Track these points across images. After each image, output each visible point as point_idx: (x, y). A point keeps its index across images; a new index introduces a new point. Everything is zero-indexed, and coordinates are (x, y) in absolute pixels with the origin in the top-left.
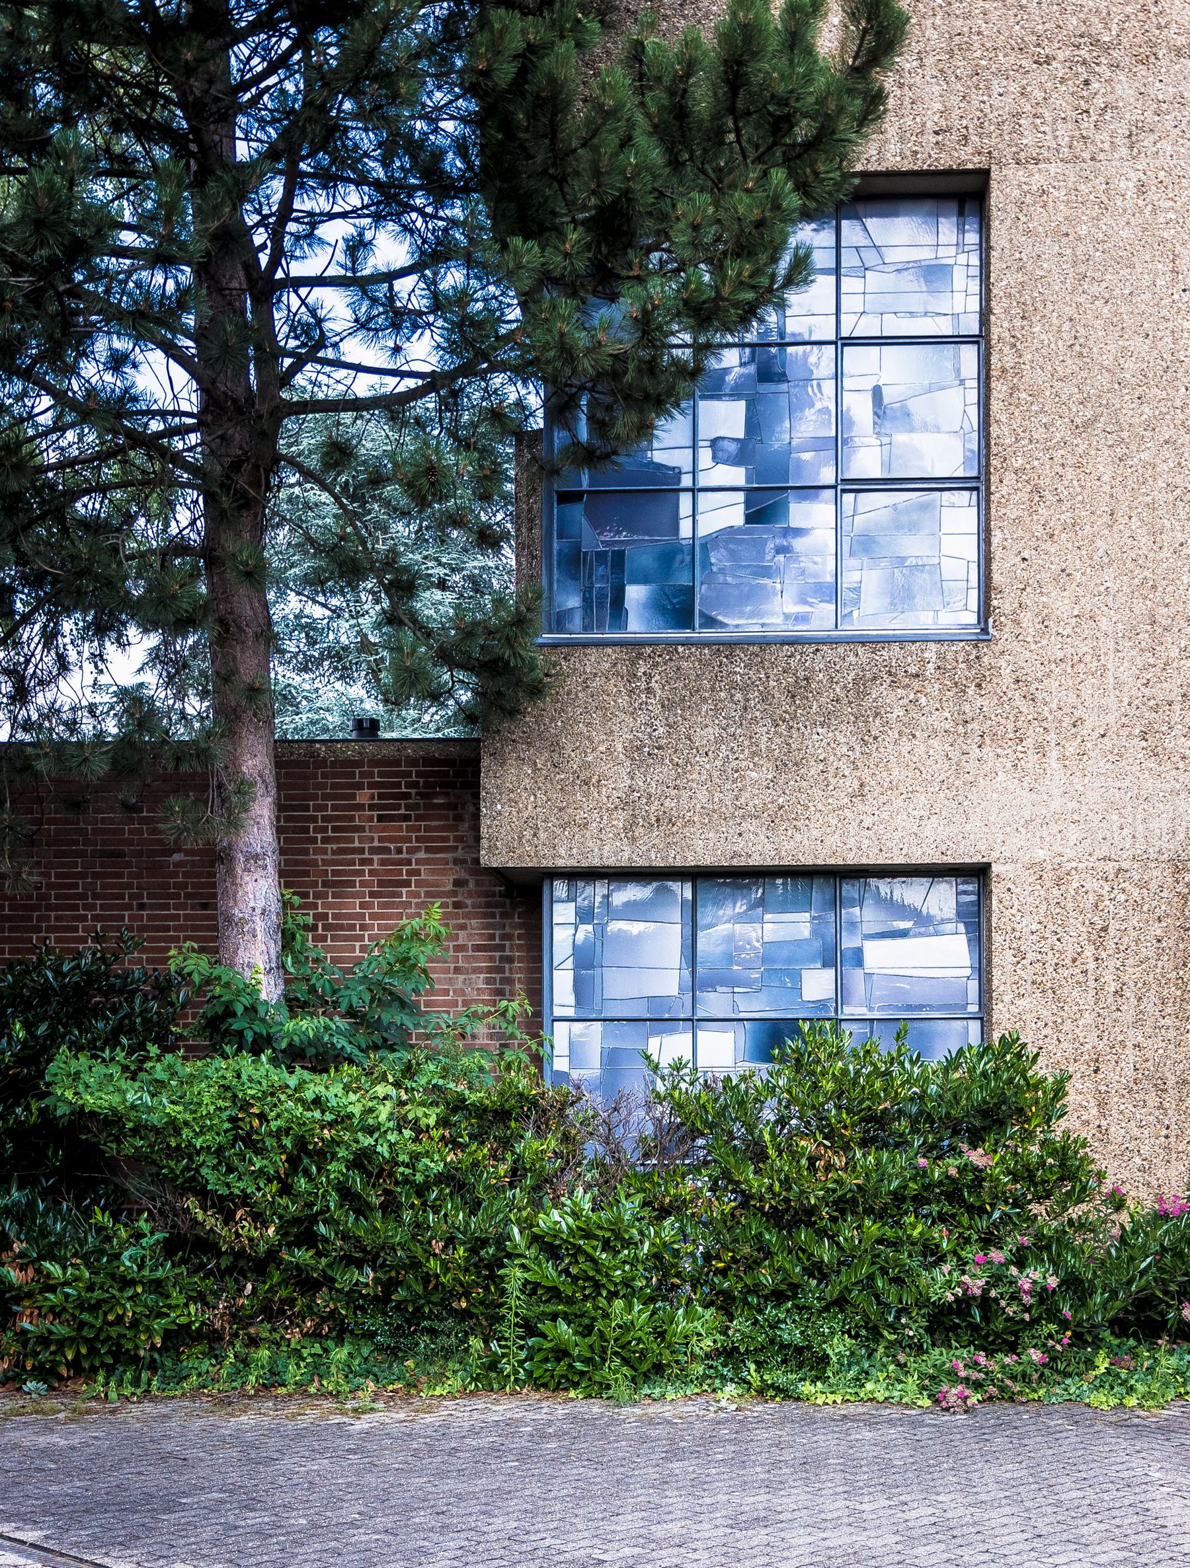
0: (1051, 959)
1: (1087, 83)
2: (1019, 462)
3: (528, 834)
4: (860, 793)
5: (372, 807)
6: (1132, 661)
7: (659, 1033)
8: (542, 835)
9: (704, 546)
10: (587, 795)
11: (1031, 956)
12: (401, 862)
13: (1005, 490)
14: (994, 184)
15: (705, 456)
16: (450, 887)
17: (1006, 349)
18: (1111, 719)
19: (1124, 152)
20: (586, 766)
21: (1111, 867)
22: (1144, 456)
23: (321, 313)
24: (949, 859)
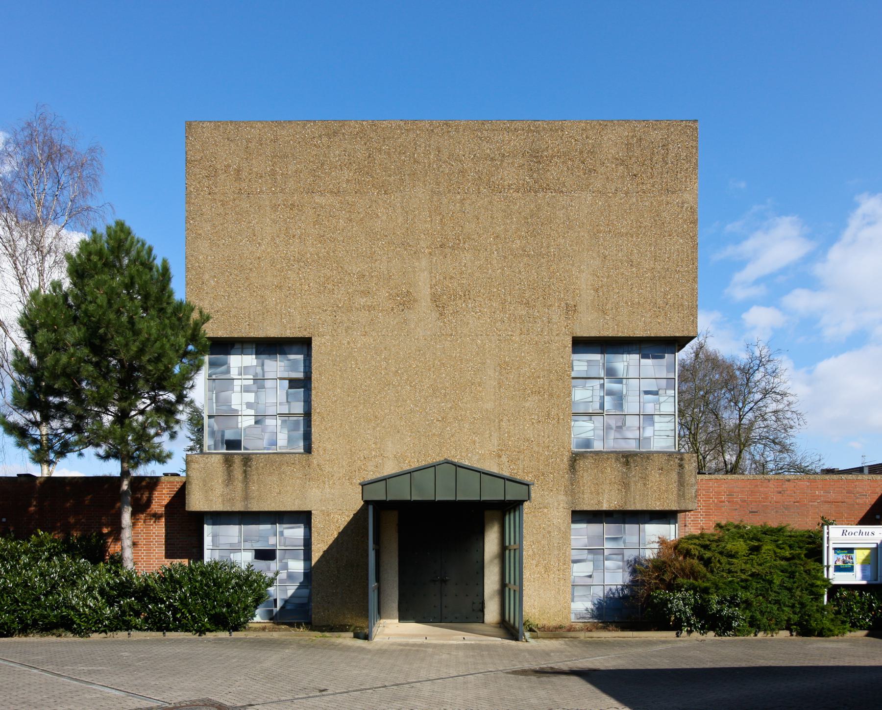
0: (326, 535)
1: (335, 316)
2: (318, 411)
3: (197, 502)
4: (279, 493)
5: (167, 494)
6: (346, 461)
8: (201, 503)
9: (245, 429)
10: (212, 493)
11: (321, 534)
13: (315, 418)
14: (313, 341)
15: (244, 407)
17: (316, 382)
18: (341, 475)
19: (345, 334)
20: (211, 485)
21: (341, 512)
22: (349, 410)
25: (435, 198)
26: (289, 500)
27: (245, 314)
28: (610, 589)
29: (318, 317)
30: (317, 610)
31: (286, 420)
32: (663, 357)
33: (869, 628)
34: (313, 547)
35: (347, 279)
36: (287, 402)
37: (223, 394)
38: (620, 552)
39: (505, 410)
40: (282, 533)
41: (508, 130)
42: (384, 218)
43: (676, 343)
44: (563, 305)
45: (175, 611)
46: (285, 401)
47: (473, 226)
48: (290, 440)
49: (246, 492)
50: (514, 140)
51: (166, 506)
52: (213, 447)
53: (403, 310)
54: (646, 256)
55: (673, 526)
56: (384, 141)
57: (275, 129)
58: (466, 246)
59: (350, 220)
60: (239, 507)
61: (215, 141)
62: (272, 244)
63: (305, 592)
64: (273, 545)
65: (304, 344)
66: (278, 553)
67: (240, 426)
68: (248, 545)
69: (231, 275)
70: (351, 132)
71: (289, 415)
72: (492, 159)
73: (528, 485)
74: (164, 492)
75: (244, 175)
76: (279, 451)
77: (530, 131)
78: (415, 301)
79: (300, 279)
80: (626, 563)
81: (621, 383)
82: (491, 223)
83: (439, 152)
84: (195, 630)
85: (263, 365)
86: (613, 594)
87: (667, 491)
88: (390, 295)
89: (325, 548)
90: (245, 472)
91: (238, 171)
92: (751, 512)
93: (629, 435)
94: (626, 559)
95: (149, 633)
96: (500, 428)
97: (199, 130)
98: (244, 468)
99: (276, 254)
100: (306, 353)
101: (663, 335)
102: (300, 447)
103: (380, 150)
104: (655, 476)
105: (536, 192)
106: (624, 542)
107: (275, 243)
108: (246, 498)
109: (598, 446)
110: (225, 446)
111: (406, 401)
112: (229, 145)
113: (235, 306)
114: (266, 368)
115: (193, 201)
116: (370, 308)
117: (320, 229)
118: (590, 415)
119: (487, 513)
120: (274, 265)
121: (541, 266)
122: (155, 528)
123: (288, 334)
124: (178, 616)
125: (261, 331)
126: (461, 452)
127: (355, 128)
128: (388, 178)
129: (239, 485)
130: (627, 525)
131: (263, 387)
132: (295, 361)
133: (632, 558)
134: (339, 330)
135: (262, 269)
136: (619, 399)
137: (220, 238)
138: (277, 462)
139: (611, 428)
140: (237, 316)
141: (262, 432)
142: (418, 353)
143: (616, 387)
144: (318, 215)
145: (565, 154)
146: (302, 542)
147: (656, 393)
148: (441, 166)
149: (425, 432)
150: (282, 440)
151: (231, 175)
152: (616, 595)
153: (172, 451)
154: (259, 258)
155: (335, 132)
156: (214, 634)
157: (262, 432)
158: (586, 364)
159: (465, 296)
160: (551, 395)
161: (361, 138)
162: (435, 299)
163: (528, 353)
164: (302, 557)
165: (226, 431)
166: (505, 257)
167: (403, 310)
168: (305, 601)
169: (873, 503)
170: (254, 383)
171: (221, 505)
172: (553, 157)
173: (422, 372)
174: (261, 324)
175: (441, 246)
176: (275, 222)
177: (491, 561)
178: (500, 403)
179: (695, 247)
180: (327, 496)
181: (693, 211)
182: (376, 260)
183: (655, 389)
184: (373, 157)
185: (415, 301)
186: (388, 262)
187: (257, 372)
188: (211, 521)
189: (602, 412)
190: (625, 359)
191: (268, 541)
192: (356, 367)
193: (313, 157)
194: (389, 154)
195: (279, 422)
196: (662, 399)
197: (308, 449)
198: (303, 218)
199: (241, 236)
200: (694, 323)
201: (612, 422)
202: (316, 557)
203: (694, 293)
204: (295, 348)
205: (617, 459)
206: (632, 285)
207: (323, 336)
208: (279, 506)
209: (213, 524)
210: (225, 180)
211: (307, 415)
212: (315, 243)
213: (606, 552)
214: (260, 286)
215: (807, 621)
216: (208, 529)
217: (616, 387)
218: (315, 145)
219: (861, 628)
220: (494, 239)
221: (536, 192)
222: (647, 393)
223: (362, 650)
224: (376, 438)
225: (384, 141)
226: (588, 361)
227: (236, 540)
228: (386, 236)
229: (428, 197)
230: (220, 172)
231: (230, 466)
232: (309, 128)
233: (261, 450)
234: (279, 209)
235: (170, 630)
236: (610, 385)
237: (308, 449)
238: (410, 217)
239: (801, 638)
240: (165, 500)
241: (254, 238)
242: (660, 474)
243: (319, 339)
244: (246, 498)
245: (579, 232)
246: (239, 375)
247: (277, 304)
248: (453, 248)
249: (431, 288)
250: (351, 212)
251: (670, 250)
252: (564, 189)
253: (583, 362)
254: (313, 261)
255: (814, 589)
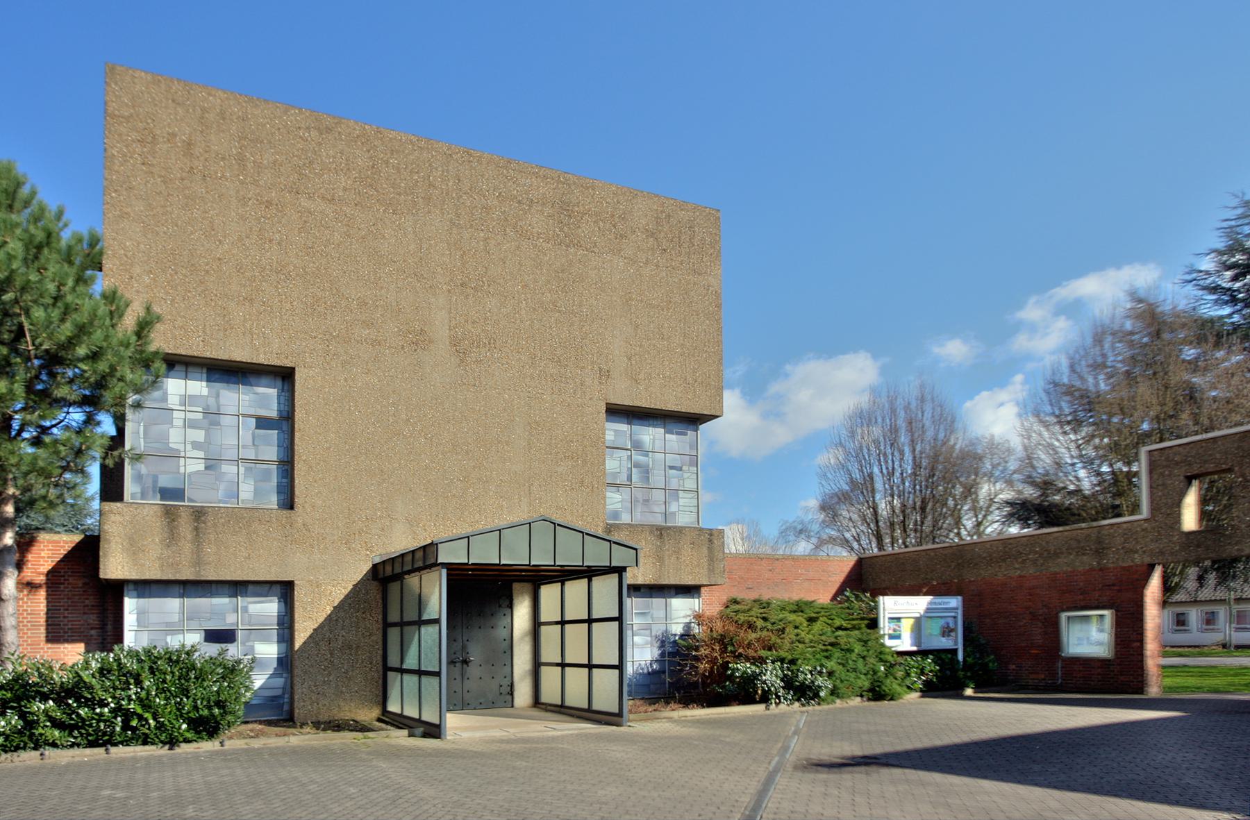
2: (304, 458)
3: (120, 567)
4: (249, 557)
5: (48, 557)
7: (172, 635)
8: (126, 568)
9: (189, 475)
12: (61, 576)
14: (296, 372)
15: (189, 447)
16: (81, 585)
18: (335, 538)
19: (340, 369)
20: (143, 545)
23: (33, 590)
24: (279, 579)
25: (455, 231)
26: (262, 566)
27: (198, 327)
28: (640, 664)
29: (304, 344)
30: (302, 704)
31: (251, 468)
32: (685, 434)
33: (921, 691)
34: (297, 626)
35: (344, 303)
36: (254, 444)
37: (156, 429)
38: (648, 627)
39: (536, 474)
40: (245, 609)
41: (537, 175)
42: (393, 240)
43: (693, 420)
44: (596, 368)
45: (127, 716)
46: (251, 444)
47: (499, 270)
48: (257, 493)
49: (198, 556)
50: (543, 188)
51: (49, 573)
52: (139, 495)
53: (415, 350)
54: (676, 331)
55: (697, 600)
56: (392, 154)
57: (244, 104)
58: (491, 290)
59: (349, 236)
60: (187, 574)
61: (154, 99)
62: (239, 245)
63: (280, 681)
64: (232, 624)
65: (285, 376)
66: (240, 634)
67: (182, 470)
68: (194, 625)
69: (176, 273)
70: (350, 134)
71: (257, 461)
72: (519, 202)
73: (636, 549)
74: (42, 555)
75: (197, 150)
76: (241, 505)
77: (559, 182)
78: (431, 341)
79: (279, 294)
80: (654, 638)
81: (647, 456)
82: (519, 269)
83: (459, 180)
84: (162, 742)
85: (218, 396)
86: (642, 669)
87: (698, 565)
88: (400, 330)
89: (316, 626)
90: (196, 529)
91: (189, 144)
92: (747, 588)
93: (656, 509)
94: (653, 634)
95: (76, 751)
96: (530, 493)
97: (128, 78)
98: (196, 524)
99: (245, 259)
100: (281, 387)
101: (692, 412)
102: (273, 500)
103: (387, 162)
104: (687, 550)
105: (567, 246)
106: (652, 618)
107: (244, 245)
108: (198, 562)
109: (625, 518)
110: (159, 495)
111: (420, 455)
112: (175, 108)
113: (182, 314)
114: (222, 401)
115: (116, 168)
116: (375, 343)
117: (308, 239)
118: (618, 486)
119: (516, 586)
120: (242, 271)
121: (572, 324)
122: (27, 603)
123: (262, 359)
124: (134, 723)
125: (222, 351)
126: (486, 517)
127: (355, 129)
128: (398, 197)
129: (187, 547)
130: (654, 600)
131: (218, 424)
132: (265, 395)
133: (659, 633)
134: (333, 364)
135: (224, 273)
136: (646, 472)
137: (159, 224)
138: (244, 518)
139: (638, 501)
140: (186, 328)
141: (216, 480)
142: (434, 401)
143: (642, 459)
144: (305, 221)
145: (596, 214)
146: (275, 621)
147: (680, 469)
148: (461, 196)
149: (443, 492)
150: (247, 491)
151: (178, 147)
152: (646, 671)
153: (1127, 287)
154: (219, 259)
155: (327, 128)
156: (194, 745)
157: (216, 480)
158: (613, 433)
159: (489, 344)
160: (585, 462)
161: (362, 143)
162: (455, 342)
163: (560, 414)
164: (275, 638)
165: (160, 476)
166: (534, 309)
167: (415, 350)
168: (279, 692)
169: (841, 581)
170: (204, 417)
171: (159, 573)
172: (584, 214)
173: (439, 424)
174: (221, 343)
175: (462, 285)
176: (243, 218)
177: (522, 638)
178: (531, 466)
179: (720, 330)
180: (317, 563)
181: (717, 295)
182: (382, 288)
183: (678, 464)
184: (378, 168)
185: (431, 341)
186: (397, 292)
187: (209, 403)
188: (135, 593)
189: (629, 483)
190: (651, 432)
191: (225, 619)
192: (356, 409)
193: (298, 150)
194: (398, 170)
195: (242, 470)
196: (686, 475)
197: (288, 502)
198: (283, 221)
199: (193, 227)
200: (721, 402)
201: (639, 494)
202: (300, 639)
203: (719, 374)
204: (264, 380)
205: (651, 532)
206: (663, 357)
207: (312, 367)
208: (248, 574)
209: (139, 597)
210: (168, 151)
211: (287, 465)
212: (300, 254)
213: (635, 628)
214: (221, 294)
215: (879, 686)
216: (130, 605)
217: (642, 459)
218: (301, 137)
219: (915, 690)
220: (523, 287)
221: (567, 246)
222: (671, 468)
223: (438, 753)
224: (383, 496)
225: (392, 154)
226: (616, 431)
227: (176, 618)
228: (394, 262)
229: (446, 228)
230: (161, 140)
231: (173, 520)
232: (292, 115)
233: (215, 503)
234: (250, 204)
235: (115, 745)
236: (637, 457)
237: (288, 502)
238: (425, 246)
239: (872, 703)
240: (44, 565)
241: (213, 233)
242: (692, 549)
243: (306, 370)
244: (198, 562)
245: (611, 296)
246: (180, 405)
247: (245, 320)
248: (475, 289)
249: (450, 330)
250: (349, 226)
251: (698, 329)
252: (595, 249)
253: (616, 431)
254: (297, 275)
255: (882, 656)
